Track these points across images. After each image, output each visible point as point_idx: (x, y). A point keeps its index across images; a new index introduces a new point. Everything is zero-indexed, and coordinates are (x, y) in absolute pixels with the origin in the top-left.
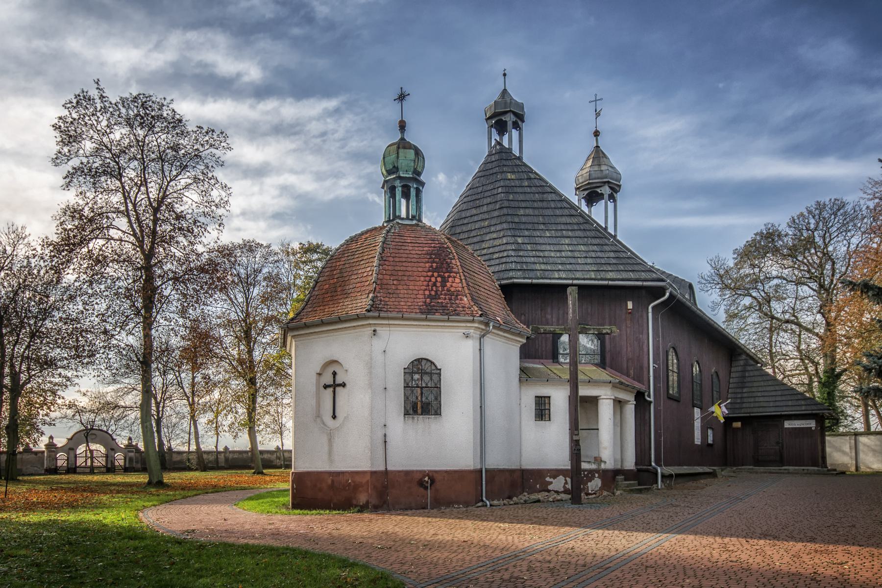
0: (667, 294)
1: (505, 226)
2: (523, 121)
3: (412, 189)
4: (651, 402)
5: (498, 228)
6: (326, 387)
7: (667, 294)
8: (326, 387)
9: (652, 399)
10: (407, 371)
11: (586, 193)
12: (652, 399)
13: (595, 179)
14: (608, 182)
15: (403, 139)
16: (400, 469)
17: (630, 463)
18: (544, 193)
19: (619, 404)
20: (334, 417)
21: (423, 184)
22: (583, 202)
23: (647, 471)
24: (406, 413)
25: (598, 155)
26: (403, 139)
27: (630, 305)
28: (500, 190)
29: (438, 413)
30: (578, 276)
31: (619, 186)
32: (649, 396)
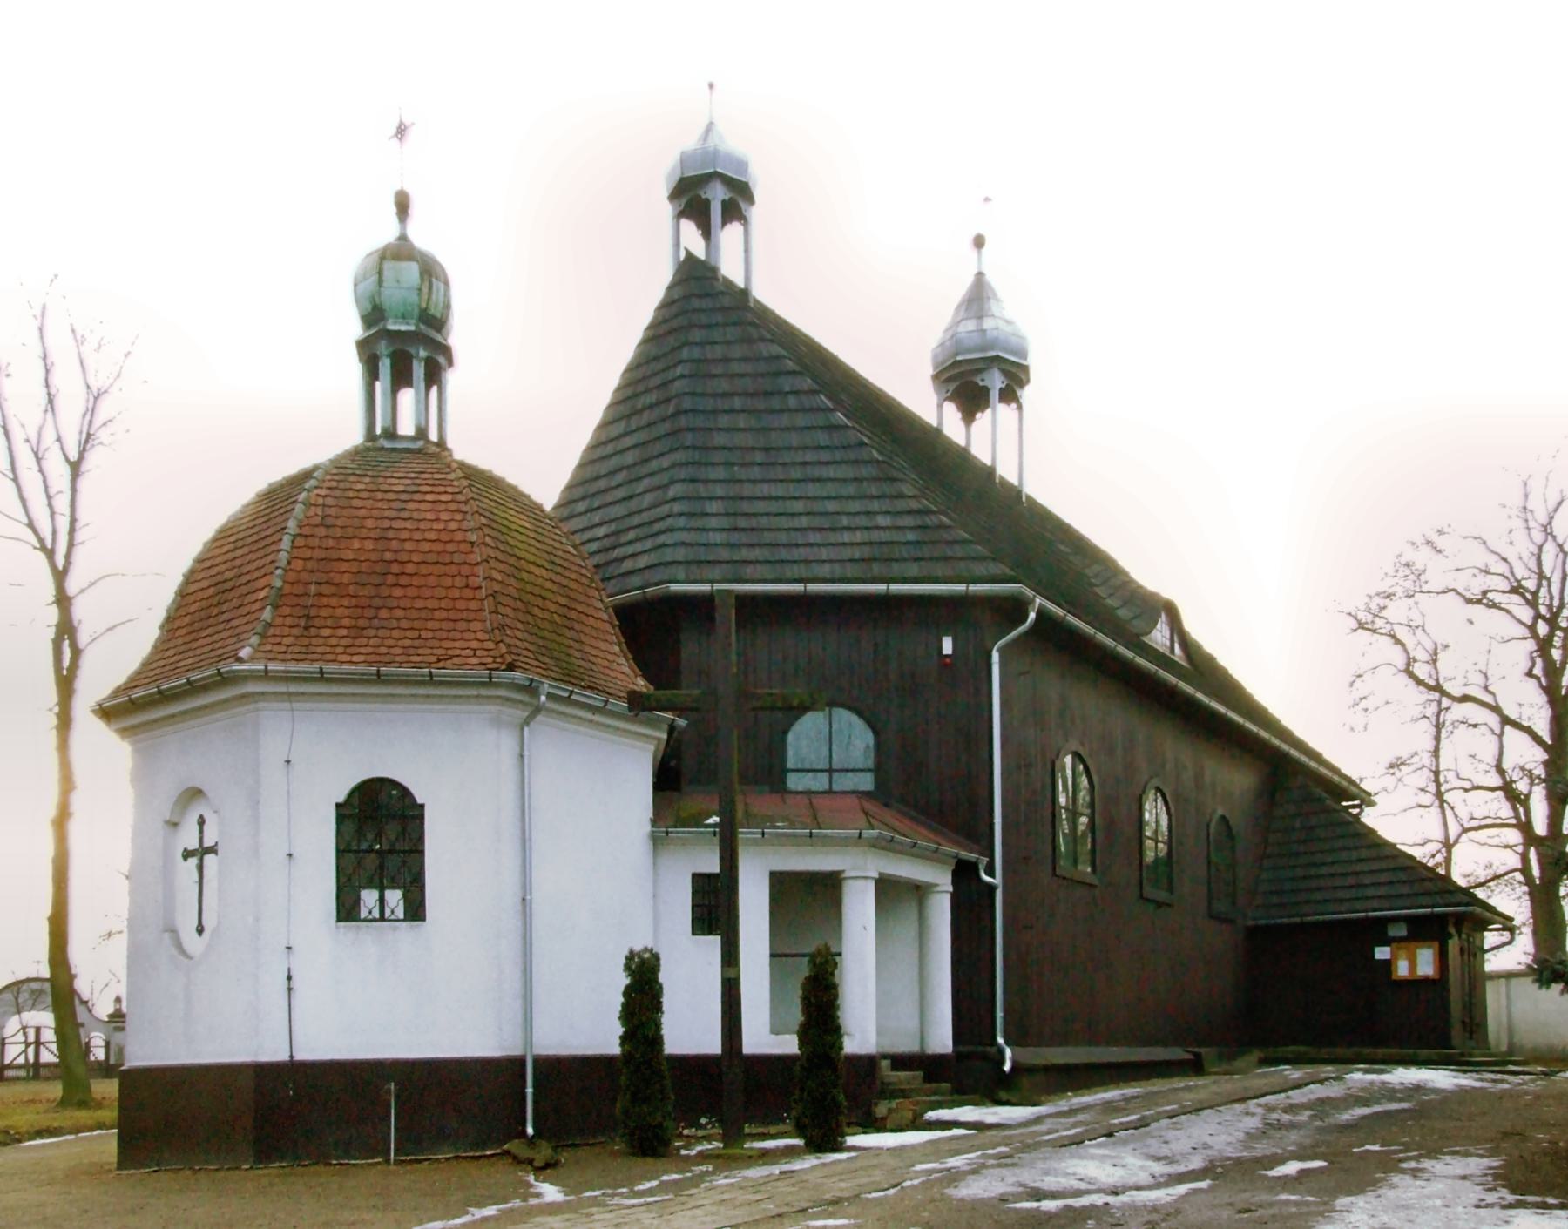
0: (1032, 616)
1: (679, 456)
2: (750, 199)
3: (415, 364)
4: (991, 889)
5: (665, 462)
6: (187, 854)
7: (1032, 616)
8: (187, 854)
9: (997, 880)
10: (346, 811)
11: (952, 386)
12: (997, 880)
13: (969, 351)
14: (998, 358)
15: (403, 238)
16: (590, 1052)
17: (942, 1040)
18: (777, 374)
19: (890, 892)
20: (200, 931)
21: (446, 351)
22: (951, 409)
23: (984, 1057)
24: (339, 919)
25: (978, 297)
26: (403, 238)
27: (947, 646)
28: (679, 370)
29: (424, 919)
30: (789, 574)
31: (1025, 369)
32: (991, 873)
